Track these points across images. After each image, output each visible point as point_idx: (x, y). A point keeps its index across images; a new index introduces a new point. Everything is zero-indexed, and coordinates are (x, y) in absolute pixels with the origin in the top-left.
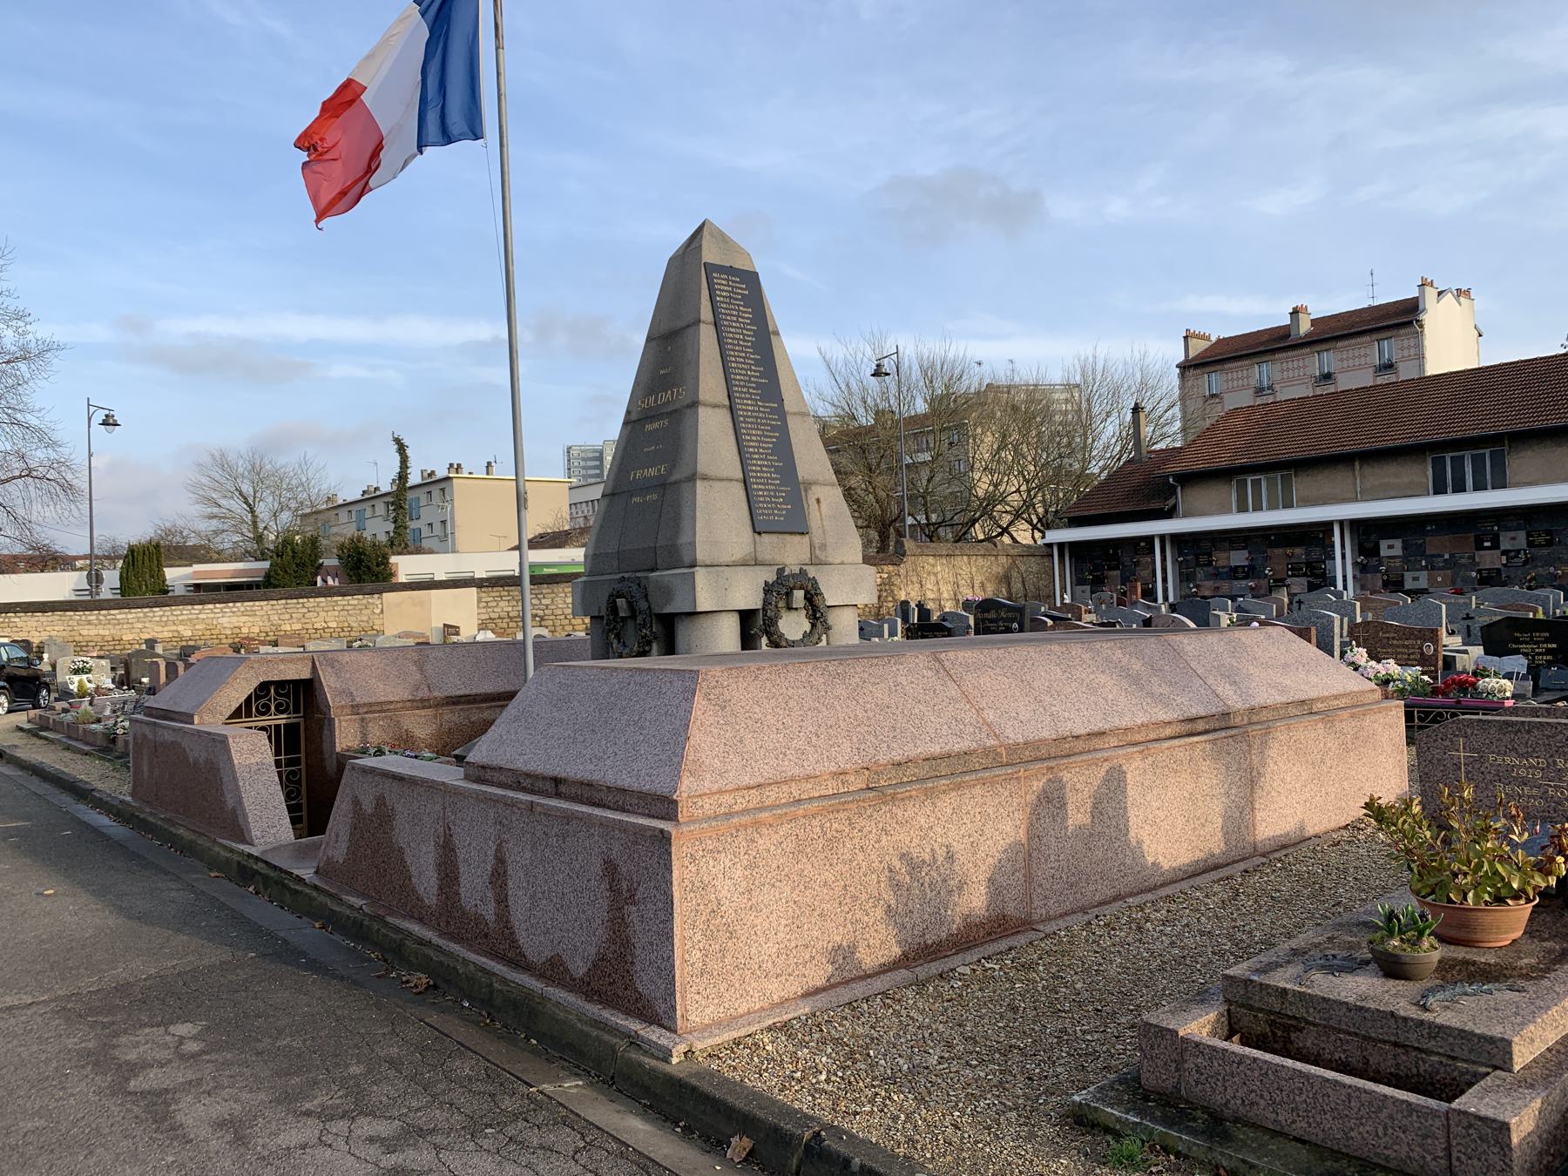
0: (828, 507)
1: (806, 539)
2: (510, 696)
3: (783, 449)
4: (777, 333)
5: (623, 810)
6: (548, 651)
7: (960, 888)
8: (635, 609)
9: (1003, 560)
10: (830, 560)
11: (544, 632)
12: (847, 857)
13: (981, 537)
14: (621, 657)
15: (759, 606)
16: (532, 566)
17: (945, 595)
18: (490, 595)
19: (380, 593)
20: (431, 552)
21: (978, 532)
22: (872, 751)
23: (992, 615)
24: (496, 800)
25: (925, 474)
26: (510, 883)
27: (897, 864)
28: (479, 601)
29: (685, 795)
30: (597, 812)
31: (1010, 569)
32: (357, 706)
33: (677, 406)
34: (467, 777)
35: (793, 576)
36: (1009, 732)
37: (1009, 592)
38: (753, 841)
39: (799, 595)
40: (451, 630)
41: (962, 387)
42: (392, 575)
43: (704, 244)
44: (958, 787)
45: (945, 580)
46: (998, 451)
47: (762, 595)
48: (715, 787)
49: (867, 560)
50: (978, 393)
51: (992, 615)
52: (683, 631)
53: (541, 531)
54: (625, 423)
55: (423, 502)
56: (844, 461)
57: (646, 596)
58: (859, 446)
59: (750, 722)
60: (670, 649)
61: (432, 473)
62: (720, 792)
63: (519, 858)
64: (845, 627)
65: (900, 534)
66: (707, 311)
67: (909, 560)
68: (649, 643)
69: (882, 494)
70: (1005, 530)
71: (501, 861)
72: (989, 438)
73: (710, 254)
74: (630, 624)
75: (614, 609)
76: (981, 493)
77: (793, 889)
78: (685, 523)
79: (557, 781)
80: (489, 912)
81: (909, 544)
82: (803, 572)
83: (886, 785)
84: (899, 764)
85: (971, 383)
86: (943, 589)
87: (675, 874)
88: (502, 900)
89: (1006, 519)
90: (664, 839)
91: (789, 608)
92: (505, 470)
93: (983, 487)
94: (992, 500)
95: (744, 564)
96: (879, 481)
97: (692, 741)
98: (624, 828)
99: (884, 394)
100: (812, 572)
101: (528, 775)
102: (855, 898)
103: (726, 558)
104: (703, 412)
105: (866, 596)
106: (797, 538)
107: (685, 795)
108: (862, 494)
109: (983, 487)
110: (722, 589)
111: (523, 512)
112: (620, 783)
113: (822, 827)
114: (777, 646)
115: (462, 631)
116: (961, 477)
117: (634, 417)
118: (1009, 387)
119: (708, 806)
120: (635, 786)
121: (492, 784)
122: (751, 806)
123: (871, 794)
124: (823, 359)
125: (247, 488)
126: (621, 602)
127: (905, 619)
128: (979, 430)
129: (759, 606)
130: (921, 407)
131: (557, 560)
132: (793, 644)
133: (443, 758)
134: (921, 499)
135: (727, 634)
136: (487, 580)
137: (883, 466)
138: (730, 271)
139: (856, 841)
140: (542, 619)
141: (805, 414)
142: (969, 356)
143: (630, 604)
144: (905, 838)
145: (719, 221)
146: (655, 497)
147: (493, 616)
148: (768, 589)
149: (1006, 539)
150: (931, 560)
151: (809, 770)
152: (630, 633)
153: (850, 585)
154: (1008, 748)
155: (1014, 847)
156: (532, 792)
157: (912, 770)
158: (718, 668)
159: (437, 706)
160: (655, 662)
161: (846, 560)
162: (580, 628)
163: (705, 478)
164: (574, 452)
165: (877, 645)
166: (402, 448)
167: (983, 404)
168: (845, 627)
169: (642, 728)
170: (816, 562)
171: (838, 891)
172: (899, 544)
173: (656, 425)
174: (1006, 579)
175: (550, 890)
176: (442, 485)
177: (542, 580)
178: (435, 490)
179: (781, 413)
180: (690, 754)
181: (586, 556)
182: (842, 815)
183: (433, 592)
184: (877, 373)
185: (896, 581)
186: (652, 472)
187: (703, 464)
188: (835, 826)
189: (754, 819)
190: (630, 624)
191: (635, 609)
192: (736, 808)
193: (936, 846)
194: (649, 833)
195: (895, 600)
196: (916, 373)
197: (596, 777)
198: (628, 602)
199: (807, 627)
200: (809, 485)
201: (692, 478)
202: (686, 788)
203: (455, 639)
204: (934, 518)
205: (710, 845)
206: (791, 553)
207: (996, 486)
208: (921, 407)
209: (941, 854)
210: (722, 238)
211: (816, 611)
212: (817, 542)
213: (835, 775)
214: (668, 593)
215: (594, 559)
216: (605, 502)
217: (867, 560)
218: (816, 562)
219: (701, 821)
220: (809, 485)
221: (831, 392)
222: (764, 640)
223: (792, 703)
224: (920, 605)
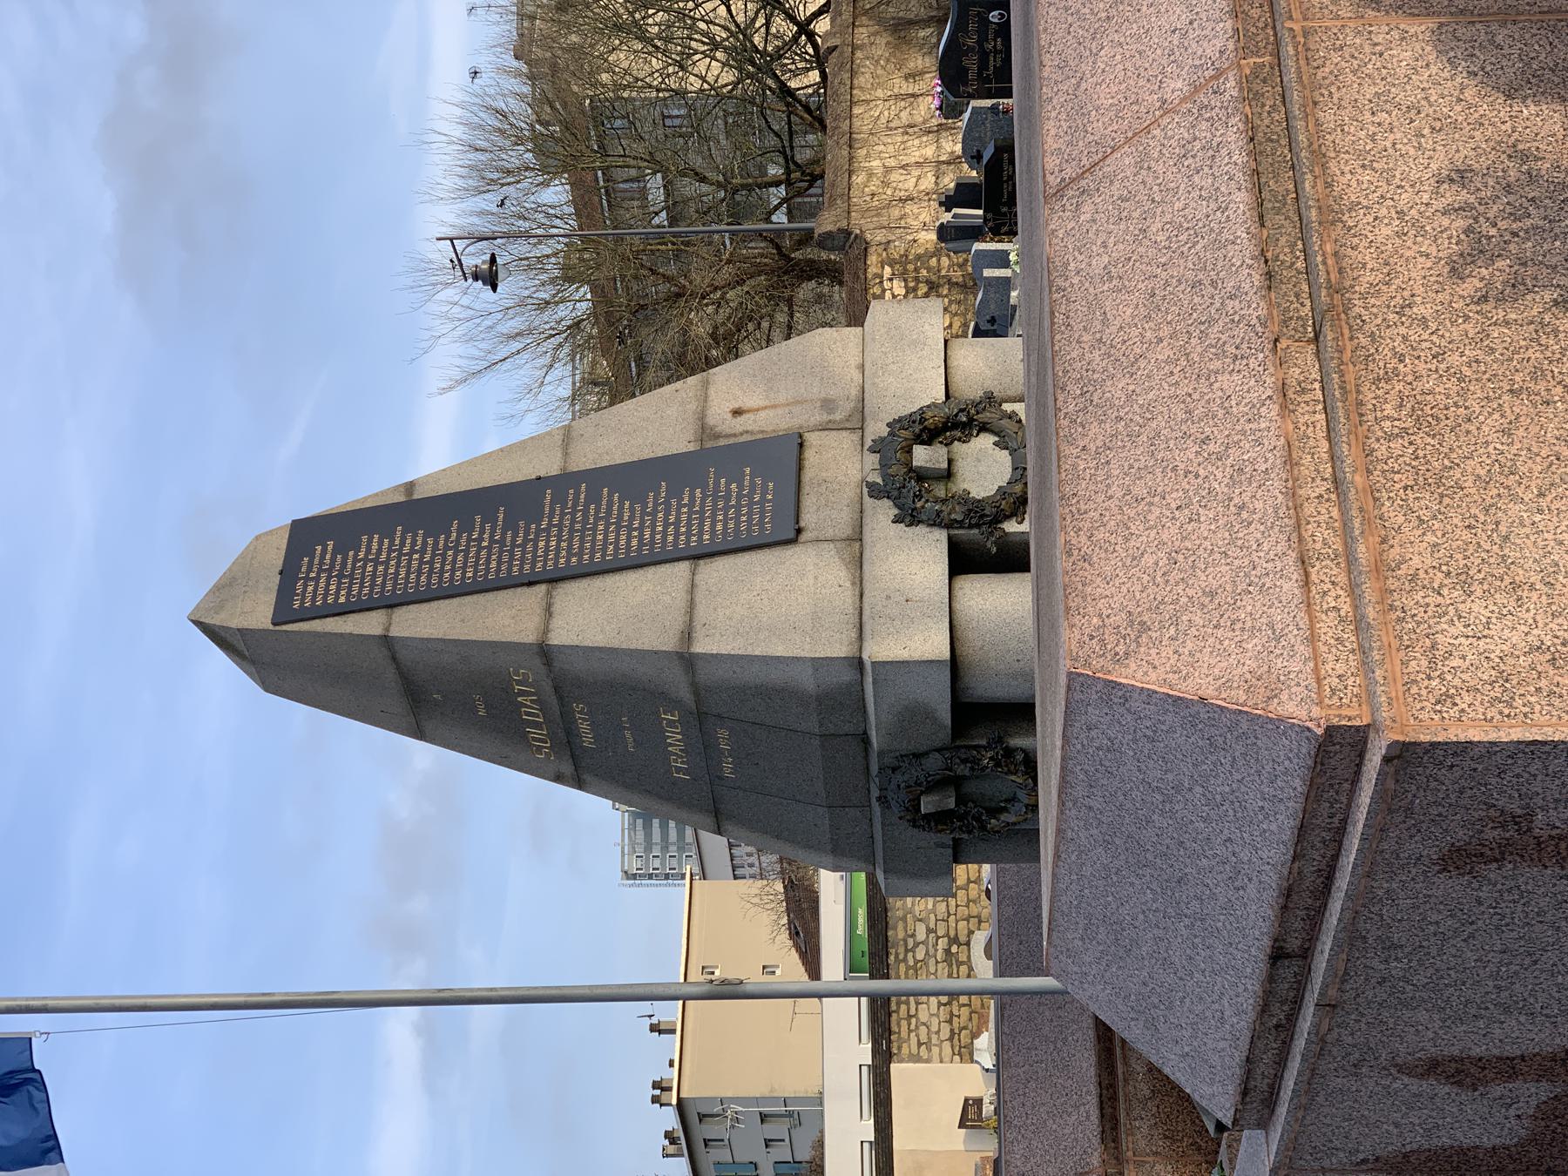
0: (748, 393)
1: (812, 438)
2: (1105, 1036)
3: (635, 479)
4: (410, 487)
5: (1340, 832)
6: (1015, 952)
7: (1525, 157)
8: (935, 780)
9: (862, 34)
10: (854, 392)
11: (980, 939)
12: (1452, 385)
13: (815, 76)
14: (1034, 808)
15: (941, 536)
16: (852, 967)
17: (929, 152)
20: (820, 1145)
21: (805, 81)
22: (1240, 331)
23: (971, 63)
24: (1311, 1073)
25: (689, 187)
26: (1476, 1051)
27: (1471, 286)
28: (916, 1059)
29: (1316, 712)
30: (1342, 882)
31: (880, 21)
33: (547, 687)
34: (1264, 1124)
35: (884, 465)
36: (1211, 50)
37: (925, 23)
38: (1414, 578)
39: (922, 456)
40: (970, 1115)
41: (521, 111)
43: (235, 623)
44: (1319, 157)
45: (900, 154)
46: (647, 40)
47: (921, 530)
48: (1303, 650)
49: (856, 318)
50: (532, 77)
51: (971, 63)
52: (988, 686)
53: (784, 936)
54: (579, 784)
55: (724, 1155)
56: (660, 346)
57: (917, 756)
58: (634, 325)
59: (1175, 576)
60: (1022, 713)
62: (1312, 639)
63: (1429, 1034)
64: (988, 365)
65: (806, 238)
66: (367, 619)
67: (858, 223)
68: (1009, 752)
69: (727, 272)
70: (804, 28)
71: (1432, 1068)
72: (621, 58)
73: (257, 613)
74: (971, 788)
75: (939, 819)
76: (728, 77)
77: (1515, 498)
78: (776, 676)
79: (1277, 955)
80: (1533, 1093)
81: (826, 223)
82: (878, 447)
83: (1310, 303)
84: (1269, 275)
85: (510, 90)
86: (915, 156)
87: (1475, 735)
88: (1510, 1068)
89: (781, 25)
90: (1403, 756)
91: (948, 475)
92: (669, 1012)
93: (715, 71)
94: (742, 52)
95: (858, 563)
96: (699, 279)
97: (1209, 692)
98: (1377, 831)
99: (531, 265)
100: (878, 428)
101: (1264, 1009)
102: (1537, 374)
103: (847, 598)
104: (563, 634)
105: (929, 321)
106: (810, 456)
107: (1316, 712)
108: (724, 312)
109: (715, 71)
110: (905, 605)
111: (749, 988)
112: (1288, 835)
113: (1390, 437)
114: (1023, 501)
115: (974, 1093)
116: (699, 111)
117: (567, 768)
118: (521, 16)
119: (1341, 665)
120: (1296, 806)
121: (1278, 1078)
122: (1342, 579)
123: (1329, 334)
124: (467, 398)
126: (928, 804)
127: (974, 233)
128: (605, 77)
129: (941, 536)
130: (557, 194)
131: (840, 909)
132: (1019, 470)
133: (1223, 1155)
134: (739, 197)
135: (998, 601)
137: (672, 269)
138: (289, 574)
139: (1421, 367)
140: (955, 940)
141: (567, 434)
142: (460, 97)
143: (934, 786)
144: (1420, 265)
145: (192, 594)
146: (723, 734)
147: (945, 1033)
148: (909, 517)
149: (822, 26)
150: (859, 179)
151: (1276, 459)
152: (996, 787)
153: (906, 352)
154: (1244, 51)
155: (1440, 40)
156: (1297, 1003)
157: (1283, 250)
158: (1065, 634)
159: (1119, 1160)
160: (1049, 740)
161: (854, 360)
162: (976, 876)
163: (688, 635)
164: (634, 865)
165: (1026, 295)
167: (554, 68)
168: (988, 365)
169: (1177, 788)
170: (857, 420)
171: (1522, 407)
172: (826, 241)
173: (584, 727)
174: (900, 29)
175: (1495, 976)
177: (877, 950)
178: (702, 1131)
179: (564, 482)
180: (1236, 697)
181: (835, 869)
182: (1368, 396)
183: (897, 1145)
184: (491, 279)
185: (898, 248)
186: (674, 737)
187: (659, 637)
188: (1389, 410)
189: (1369, 575)
190: (971, 788)
191: (935, 780)
192: (1346, 608)
193: (1438, 204)
194: (1391, 784)
195: (937, 253)
196: (489, 202)
197: (1273, 880)
198: (929, 790)
199: (985, 441)
200: (704, 431)
201: (687, 661)
202: (1298, 707)
203: (988, 1109)
204: (774, 171)
205: (1419, 663)
206: (839, 468)
207: (715, 45)
208: (557, 194)
209: (1453, 195)
210: (225, 588)
211: (955, 422)
212: (819, 417)
213: (1286, 408)
214: (914, 714)
215: (842, 854)
216: (728, 827)
217: (856, 318)
218: (857, 420)
219: (1370, 683)
220: (704, 431)
221: (526, 369)
222: (1011, 527)
223: (1140, 490)
224: (948, 203)
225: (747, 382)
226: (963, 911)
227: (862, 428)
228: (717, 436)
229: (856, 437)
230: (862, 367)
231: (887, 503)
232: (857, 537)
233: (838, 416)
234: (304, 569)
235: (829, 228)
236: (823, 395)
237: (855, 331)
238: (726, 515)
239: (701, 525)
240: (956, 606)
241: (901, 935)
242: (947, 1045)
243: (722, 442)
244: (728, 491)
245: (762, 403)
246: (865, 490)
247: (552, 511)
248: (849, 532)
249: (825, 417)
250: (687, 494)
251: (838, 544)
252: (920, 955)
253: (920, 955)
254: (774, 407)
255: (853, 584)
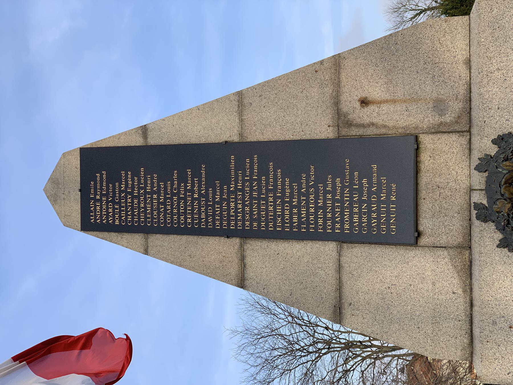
1: (426, 140)
10: (462, 91)
95: (468, 272)
106: (425, 158)
161: (461, 56)
212: (430, 119)
218: (464, 126)
225: (371, 71)
227: (469, 131)
228: (349, 124)
229: (463, 140)
230: (468, 62)
231: (491, 226)
232: (466, 246)
233: (448, 118)
234: (92, 191)
235: (484, 174)
236: (435, 95)
237: (459, 21)
238: (360, 208)
239: (342, 215)
244: (361, 185)
246: (474, 212)
248: (460, 240)
249: (438, 119)
250: (329, 182)
251: (451, 251)
254: (394, 101)
255: (465, 291)
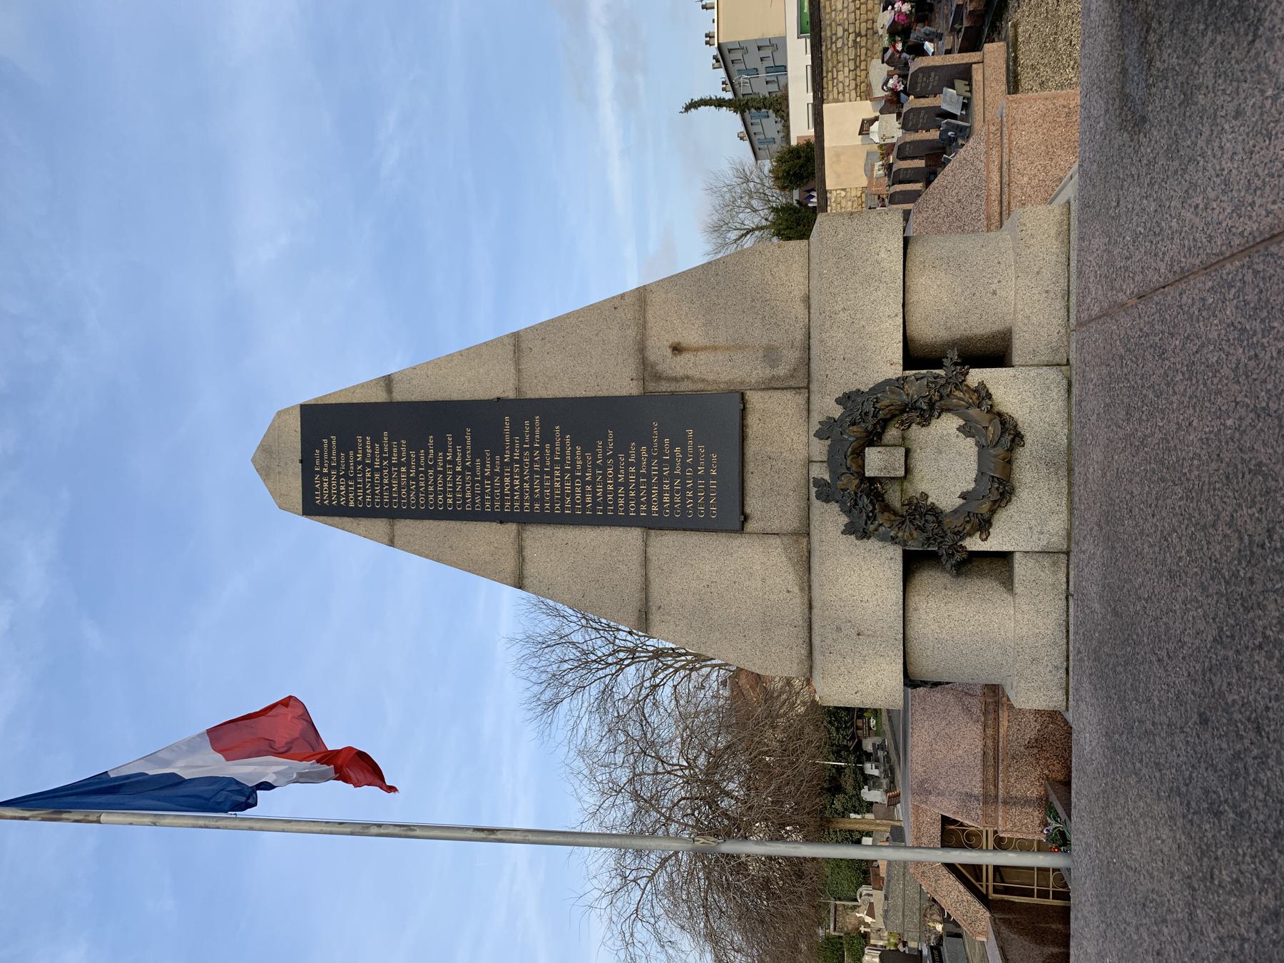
1: (754, 398)
10: (799, 336)
18: (831, 90)
19: (826, 192)
28: (837, 101)
32: (985, 795)
42: (808, 144)
47: (873, 544)
61: (715, 57)
95: (806, 564)
103: (796, 603)
125: (733, 235)
136: (814, 92)
147: (853, 85)
166: (694, 105)
176: (726, 52)
178: (730, 57)
206: (785, 439)
212: (760, 372)
218: (801, 381)
226: (864, 17)
227: (808, 388)
229: (800, 399)
230: (807, 300)
231: (835, 507)
232: (804, 532)
234: (317, 462)
236: (765, 342)
240: (911, 633)
241: (829, 34)
242: (853, 93)
243: (664, 387)
244: (673, 455)
245: (703, 342)
246: (813, 490)
247: (512, 442)
248: (796, 524)
249: (768, 372)
252: (839, 45)
253: (839, 45)
254: (715, 348)
255: (802, 590)
